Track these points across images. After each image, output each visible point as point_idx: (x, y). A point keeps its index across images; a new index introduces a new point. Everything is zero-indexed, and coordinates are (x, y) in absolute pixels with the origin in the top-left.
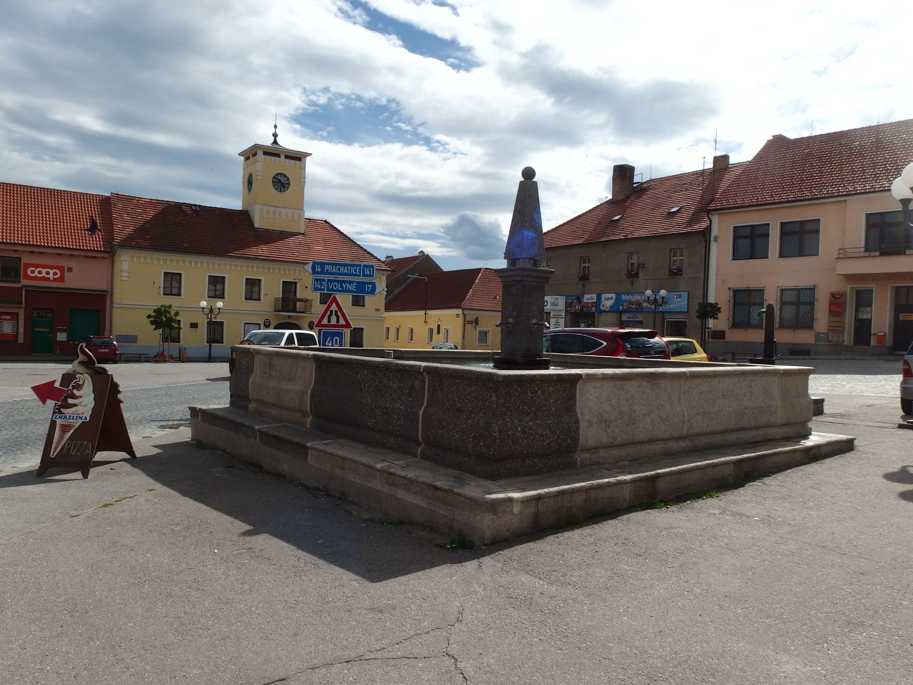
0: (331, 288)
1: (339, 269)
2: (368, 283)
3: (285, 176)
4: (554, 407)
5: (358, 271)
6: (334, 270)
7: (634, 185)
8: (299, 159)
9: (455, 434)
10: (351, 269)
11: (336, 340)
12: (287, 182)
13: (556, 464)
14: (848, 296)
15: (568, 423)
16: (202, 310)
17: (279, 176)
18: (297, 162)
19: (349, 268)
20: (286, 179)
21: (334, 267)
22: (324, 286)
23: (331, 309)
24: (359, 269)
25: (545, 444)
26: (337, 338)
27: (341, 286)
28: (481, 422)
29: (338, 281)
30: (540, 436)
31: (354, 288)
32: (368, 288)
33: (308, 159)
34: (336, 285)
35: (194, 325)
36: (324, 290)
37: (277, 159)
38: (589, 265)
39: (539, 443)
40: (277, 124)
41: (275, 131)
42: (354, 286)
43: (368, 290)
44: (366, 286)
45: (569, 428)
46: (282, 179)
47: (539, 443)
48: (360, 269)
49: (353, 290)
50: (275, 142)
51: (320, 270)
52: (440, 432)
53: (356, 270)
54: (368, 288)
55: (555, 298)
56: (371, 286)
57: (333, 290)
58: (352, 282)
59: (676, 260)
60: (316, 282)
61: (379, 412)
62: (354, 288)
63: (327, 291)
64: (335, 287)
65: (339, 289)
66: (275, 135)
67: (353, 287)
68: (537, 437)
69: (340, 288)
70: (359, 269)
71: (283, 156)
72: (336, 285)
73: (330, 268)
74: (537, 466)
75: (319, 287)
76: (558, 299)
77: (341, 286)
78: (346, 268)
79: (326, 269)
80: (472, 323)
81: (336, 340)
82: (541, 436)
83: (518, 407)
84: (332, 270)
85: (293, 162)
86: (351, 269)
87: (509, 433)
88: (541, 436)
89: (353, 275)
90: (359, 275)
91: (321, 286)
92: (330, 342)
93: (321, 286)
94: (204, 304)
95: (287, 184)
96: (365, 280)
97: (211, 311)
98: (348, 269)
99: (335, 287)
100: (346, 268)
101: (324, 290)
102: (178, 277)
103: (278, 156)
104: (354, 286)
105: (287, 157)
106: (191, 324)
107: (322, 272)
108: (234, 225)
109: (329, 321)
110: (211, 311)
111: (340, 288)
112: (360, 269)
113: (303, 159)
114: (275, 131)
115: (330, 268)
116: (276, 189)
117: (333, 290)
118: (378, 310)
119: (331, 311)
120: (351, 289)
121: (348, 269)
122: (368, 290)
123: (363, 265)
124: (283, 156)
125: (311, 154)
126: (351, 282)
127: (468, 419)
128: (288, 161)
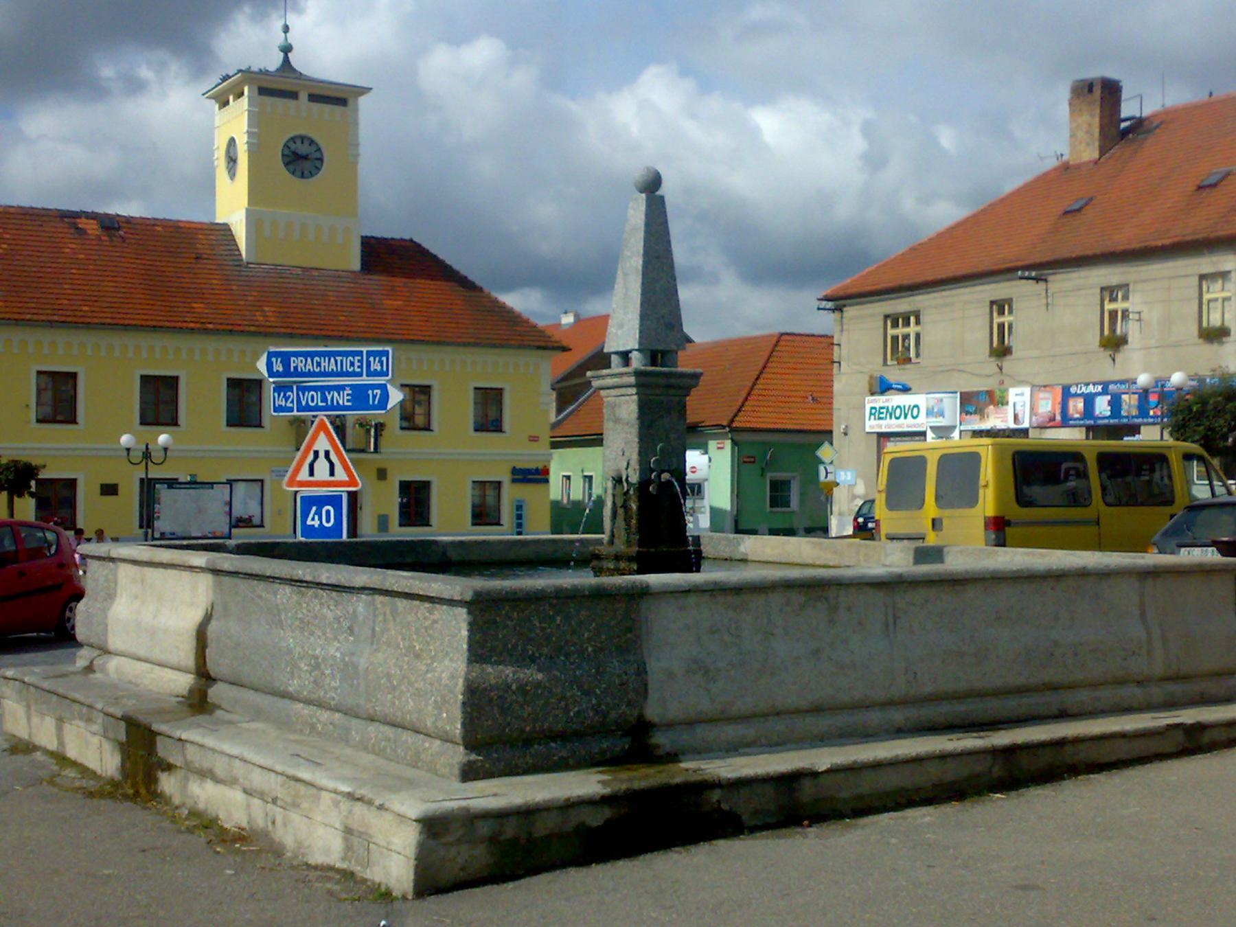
0: (304, 403)
1: (319, 364)
2: (373, 387)
3: (312, 142)
4: (591, 646)
5: (357, 364)
6: (309, 367)
7: (1123, 125)
8: (342, 102)
9: (410, 700)
10: (342, 361)
11: (328, 512)
12: (318, 155)
13: (596, 751)
14: (344, 452)
15: (619, 676)
16: (125, 453)
17: (299, 142)
18: (338, 109)
19: (339, 359)
20: (314, 148)
21: (309, 360)
22: (292, 402)
23: (315, 449)
24: (359, 361)
25: (572, 714)
26: (329, 507)
27: (324, 399)
28: (444, 675)
29: (315, 389)
30: (560, 700)
31: (348, 401)
32: (374, 397)
33: (363, 101)
34: (313, 397)
35: (109, 490)
36: (291, 410)
37: (291, 103)
38: (918, 329)
39: (557, 712)
40: (288, 23)
41: (286, 39)
42: (348, 395)
43: (374, 401)
44: (370, 392)
45: (622, 684)
46: (303, 149)
47: (557, 712)
48: (361, 361)
49: (346, 404)
50: (286, 61)
51: (281, 369)
52: (389, 697)
53: (352, 364)
54: (374, 397)
55: (937, 399)
56: (379, 392)
57: (308, 408)
58: (343, 388)
59: (1216, 300)
60: (276, 395)
61: (305, 665)
62: (348, 401)
63: (298, 411)
64: (313, 401)
65: (320, 404)
66: (287, 49)
67: (346, 398)
68: (553, 700)
69: (322, 402)
70: (359, 361)
71: (303, 96)
72: (313, 397)
73: (301, 361)
74: (554, 755)
75: (283, 404)
76: (941, 400)
77: (324, 399)
78: (332, 360)
79: (292, 365)
80: (754, 462)
81: (328, 512)
82: (563, 698)
83: (515, 647)
84: (305, 366)
85: (327, 108)
86: (342, 361)
87: (492, 694)
88: (563, 698)
89: (348, 374)
90: (360, 375)
91: (286, 402)
92: (316, 517)
93: (286, 402)
94: (125, 439)
95: (317, 159)
96: (365, 380)
97: (147, 455)
98: (336, 361)
99: (313, 401)
100: (332, 360)
101: (291, 410)
102: (71, 382)
103: (294, 95)
104: (348, 395)
105: (314, 98)
106: (102, 486)
107: (287, 373)
108: (197, 258)
109: (312, 473)
110: (147, 455)
111: (322, 402)
112: (361, 361)
113: (350, 102)
114: (286, 39)
115: (301, 361)
116: (293, 173)
117: (308, 408)
118: (534, 439)
119: (316, 454)
120: (341, 402)
121: (336, 361)
122: (374, 401)
123: (367, 352)
124: (303, 96)
125: (371, 89)
126: (340, 388)
127: (427, 671)
128: (316, 107)
